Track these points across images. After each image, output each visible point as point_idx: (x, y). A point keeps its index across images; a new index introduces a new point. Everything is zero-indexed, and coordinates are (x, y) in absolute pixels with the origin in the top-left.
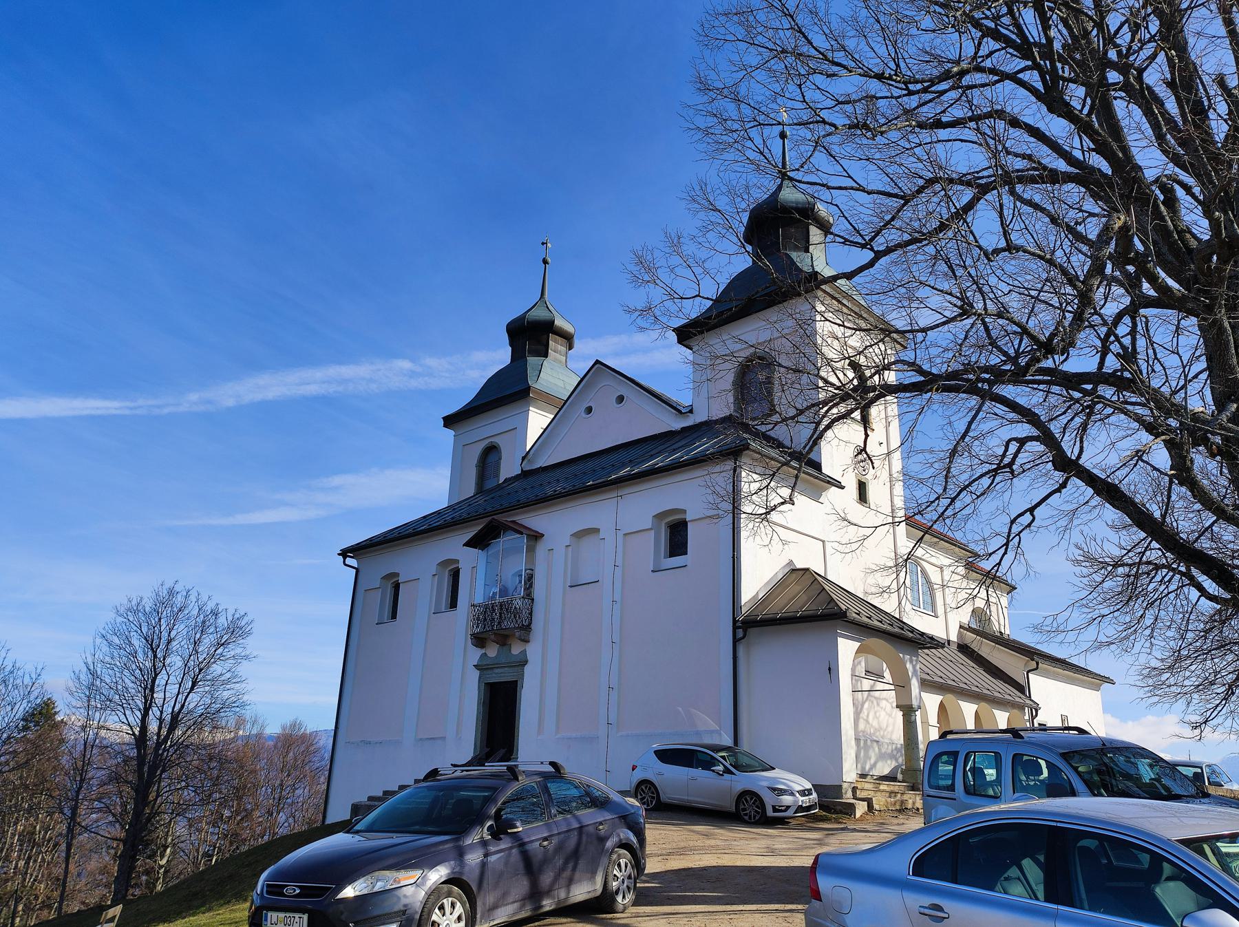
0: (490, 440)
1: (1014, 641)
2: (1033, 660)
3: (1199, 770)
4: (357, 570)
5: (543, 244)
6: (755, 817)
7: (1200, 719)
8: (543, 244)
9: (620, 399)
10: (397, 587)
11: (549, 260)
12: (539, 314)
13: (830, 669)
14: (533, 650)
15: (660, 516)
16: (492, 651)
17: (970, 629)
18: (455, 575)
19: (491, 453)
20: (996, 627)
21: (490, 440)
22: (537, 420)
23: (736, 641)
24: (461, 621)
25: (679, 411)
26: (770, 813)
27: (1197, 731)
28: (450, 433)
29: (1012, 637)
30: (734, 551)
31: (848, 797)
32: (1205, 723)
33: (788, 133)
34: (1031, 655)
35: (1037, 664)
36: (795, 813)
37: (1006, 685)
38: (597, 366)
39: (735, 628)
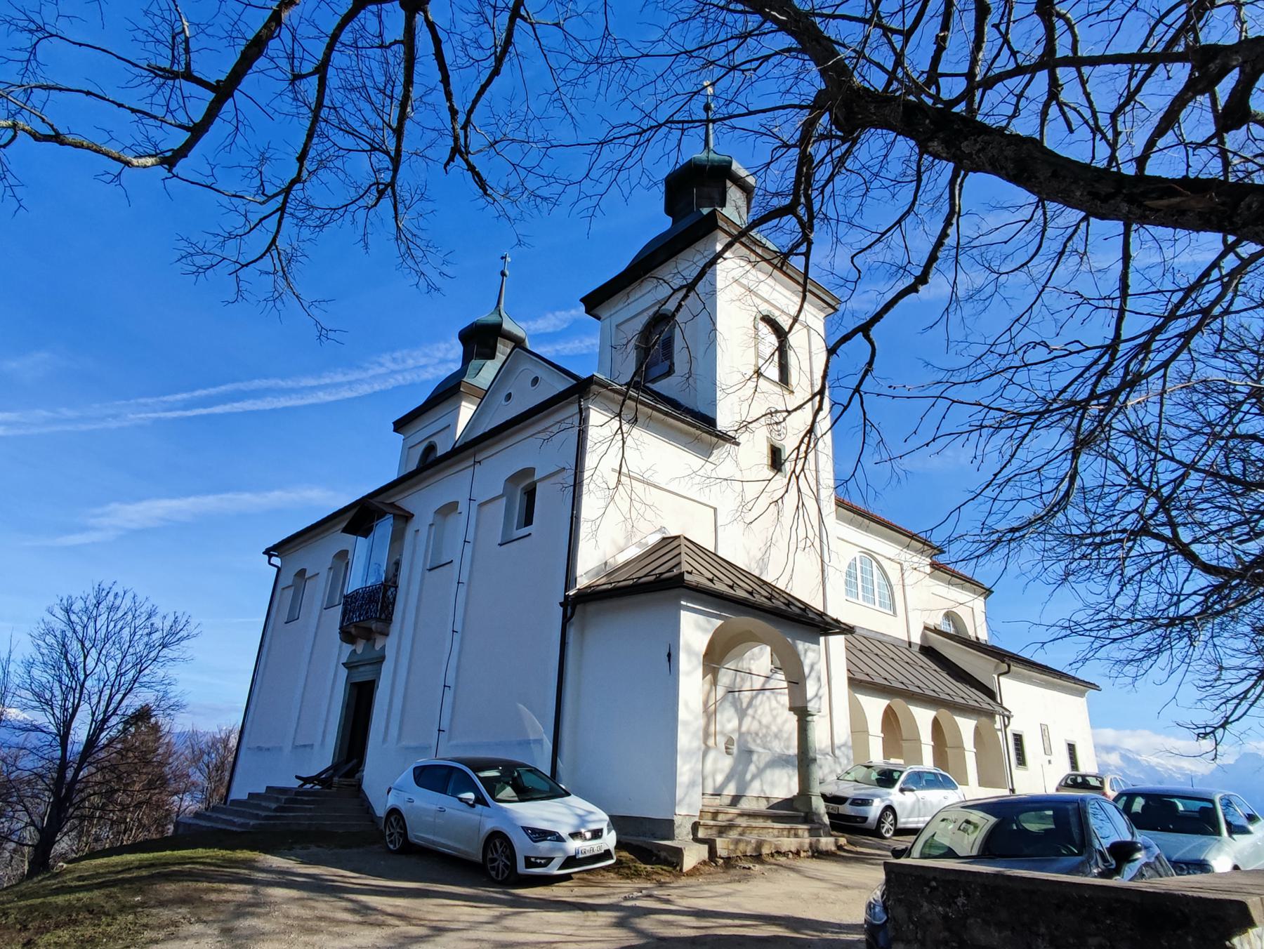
1: (993, 647)
2: (1003, 662)
3: (1210, 805)
4: (279, 569)
5: (502, 258)
6: (503, 872)
7: (1217, 719)
8: (502, 258)
11: (507, 273)
14: (390, 644)
17: (936, 631)
20: (971, 633)
22: (467, 411)
23: (566, 620)
26: (521, 868)
27: (1207, 744)
29: (990, 643)
30: (573, 510)
31: (682, 836)
32: (1223, 726)
33: (712, 106)
34: (1006, 659)
35: (1009, 666)
36: (562, 867)
37: (973, 690)
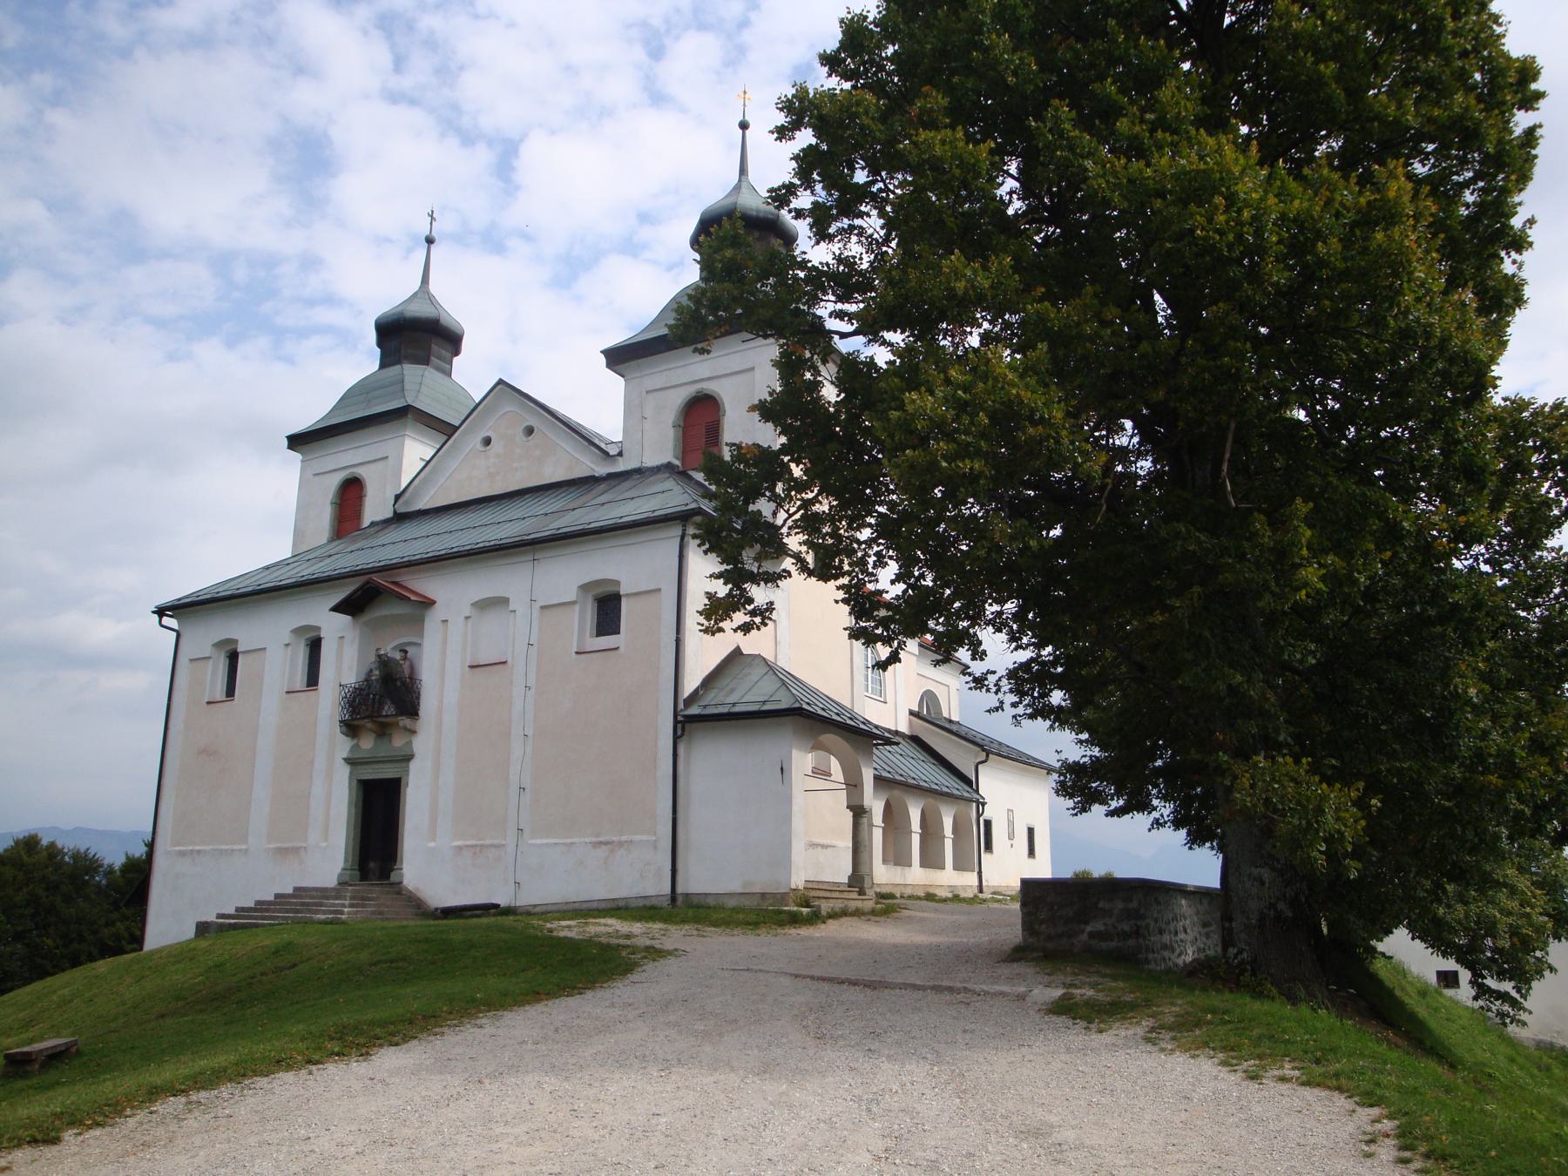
0: (352, 470)
9: (530, 431)
10: (233, 657)
12: (421, 310)
13: (782, 769)
14: (422, 744)
15: (585, 588)
16: (367, 743)
18: (315, 646)
19: (351, 490)
21: (352, 470)
23: (676, 739)
24: (328, 702)
25: (606, 454)
28: (296, 457)
38: (500, 386)
39: (676, 722)
